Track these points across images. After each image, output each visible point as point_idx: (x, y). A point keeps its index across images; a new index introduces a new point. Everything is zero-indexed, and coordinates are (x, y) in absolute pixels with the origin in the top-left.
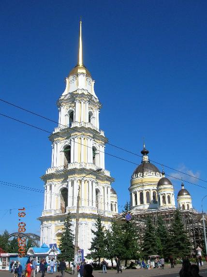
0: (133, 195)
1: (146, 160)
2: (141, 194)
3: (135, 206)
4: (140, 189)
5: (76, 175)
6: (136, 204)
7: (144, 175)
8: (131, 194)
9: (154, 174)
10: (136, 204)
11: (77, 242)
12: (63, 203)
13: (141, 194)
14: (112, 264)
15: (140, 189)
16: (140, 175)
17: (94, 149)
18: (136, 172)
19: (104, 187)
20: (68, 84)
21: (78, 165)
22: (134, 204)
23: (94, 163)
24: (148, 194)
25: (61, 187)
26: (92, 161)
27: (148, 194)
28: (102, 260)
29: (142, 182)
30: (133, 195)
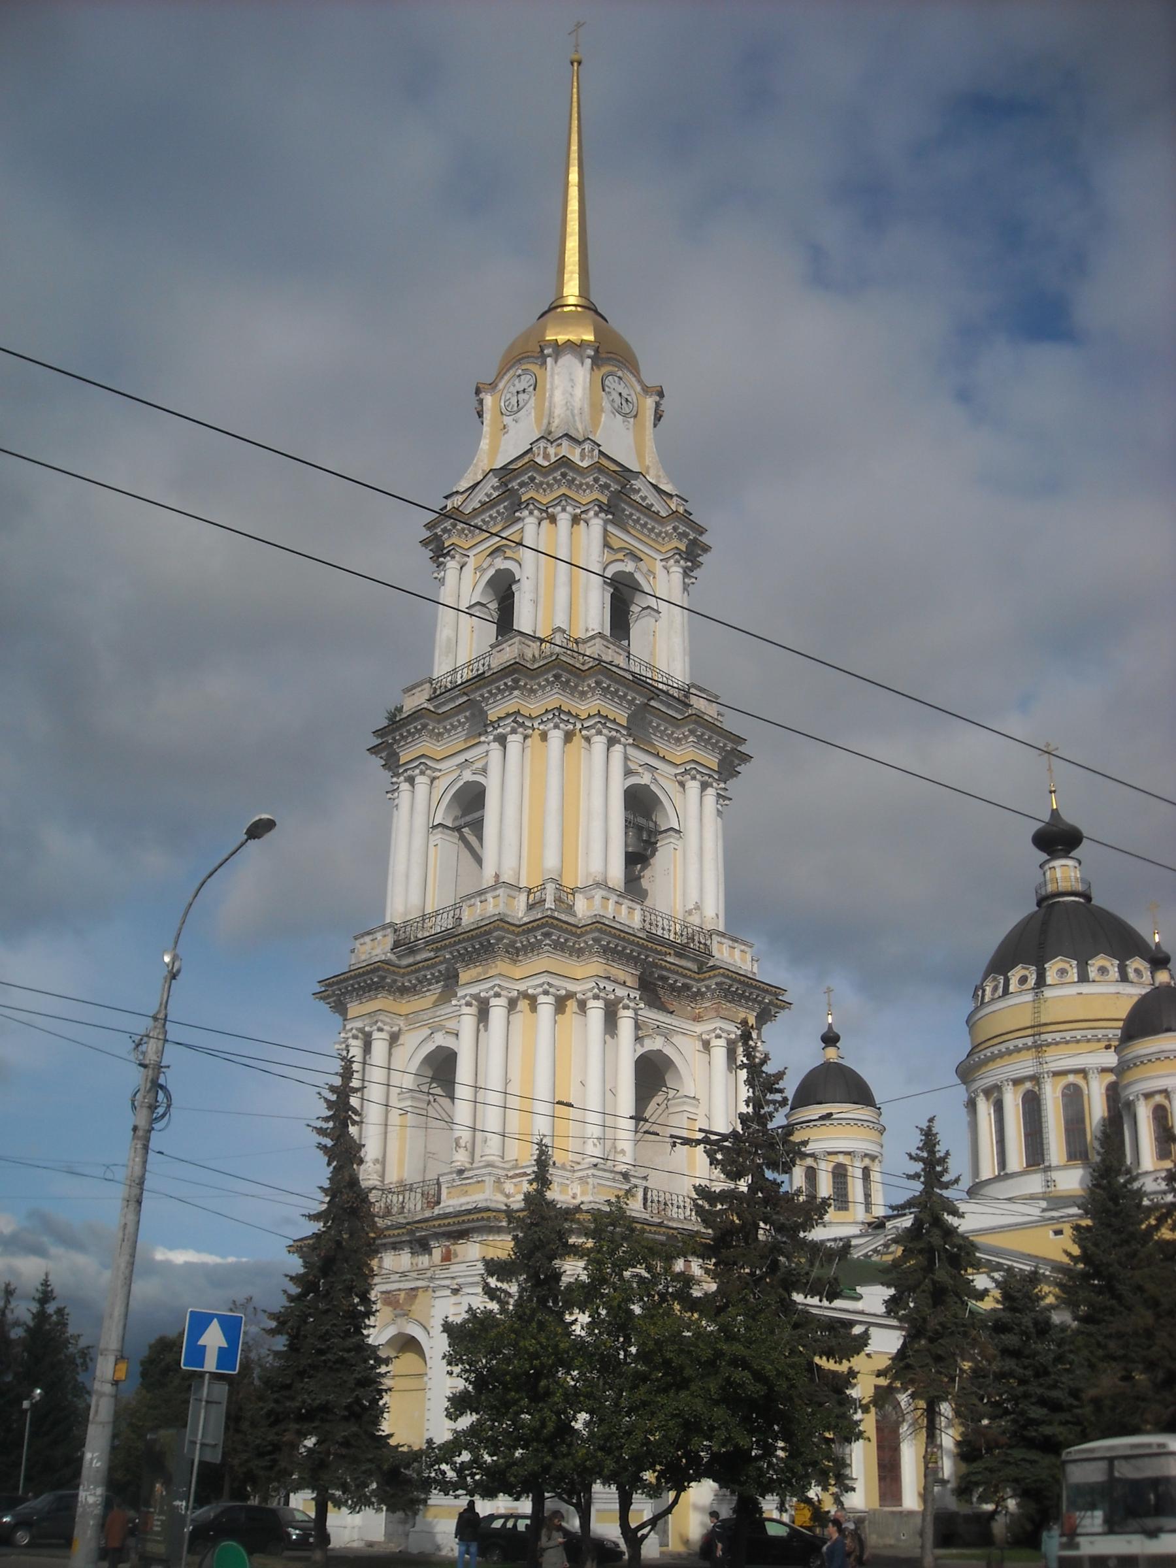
0: (985, 1109)
2: (1033, 1106)
4: (1024, 1065)
6: (1002, 1163)
7: (1051, 977)
8: (972, 1105)
9: (1114, 973)
10: (1002, 1163)
12: (131, 1217)
13: (1033, 1106)
14: (1032, 1197)
15: (1024, 1065)
17: (646, 1132)
18: (1001, 964)
21: (522, 900)
23: (633, 888)
24: (1074, 1099)
26: (616, 873)
27: (1074, 1099)
28: (743, 1186)
29: (1038, 1028)
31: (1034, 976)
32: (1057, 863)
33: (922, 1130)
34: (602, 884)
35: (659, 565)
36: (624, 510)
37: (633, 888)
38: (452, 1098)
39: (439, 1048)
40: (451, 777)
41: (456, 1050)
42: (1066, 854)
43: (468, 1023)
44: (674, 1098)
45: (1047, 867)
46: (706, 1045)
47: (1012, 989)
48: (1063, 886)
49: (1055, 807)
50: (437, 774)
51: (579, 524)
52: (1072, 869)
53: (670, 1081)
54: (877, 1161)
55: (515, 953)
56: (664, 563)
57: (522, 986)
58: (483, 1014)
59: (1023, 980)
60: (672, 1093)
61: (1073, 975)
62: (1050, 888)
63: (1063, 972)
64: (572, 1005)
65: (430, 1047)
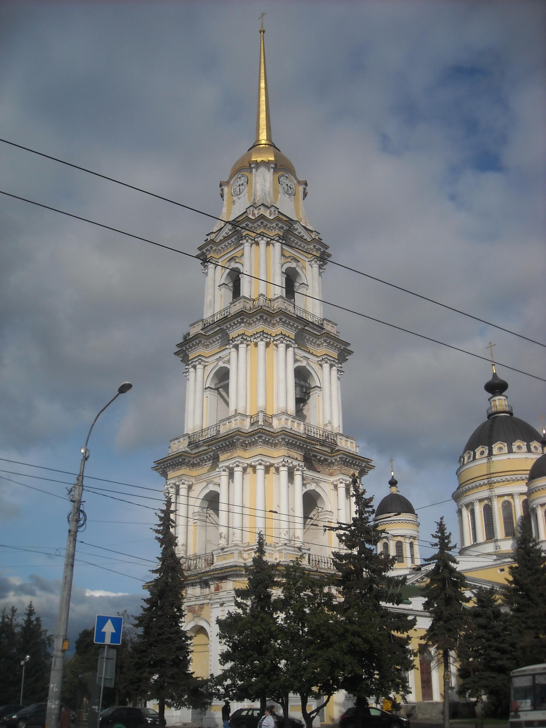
0: (466, 514)
1: (497, 403)
3: (473, 546)
5: (239, 452)
6: (475, 539)
7: (495, 451)
8: (460, 512)
9: (524, 449)
10: (475, 539)
11: (404, 701)
15: (484, 493)
16: (500, 449)
18: (471, 446)
19: (336, 487)
20: (107, 651)
21: (248, 421)
22: (468, 542)
23: (300, 414)
24: (507, 508)
25: (207, 491)
26: (292, 408)
27: (507, 508)
29: (490, 475)
30: (466, 514)
31: (487, 451)
32: (496, 398)
34: (285, 413)
37: (300, 414)
40: (213, 365)
42: (500, 394)
43: (224, 479)
44: (321, 512)
47: (477, 457)
48: (499, 409)
50: (207, 364)
55: (245, 446)
56: (310, 263)
57: (249, 462)
58: (231, 475)
59: (482, 453)
60: (320, 510)
62: (494, 410)
64: (272, 470)
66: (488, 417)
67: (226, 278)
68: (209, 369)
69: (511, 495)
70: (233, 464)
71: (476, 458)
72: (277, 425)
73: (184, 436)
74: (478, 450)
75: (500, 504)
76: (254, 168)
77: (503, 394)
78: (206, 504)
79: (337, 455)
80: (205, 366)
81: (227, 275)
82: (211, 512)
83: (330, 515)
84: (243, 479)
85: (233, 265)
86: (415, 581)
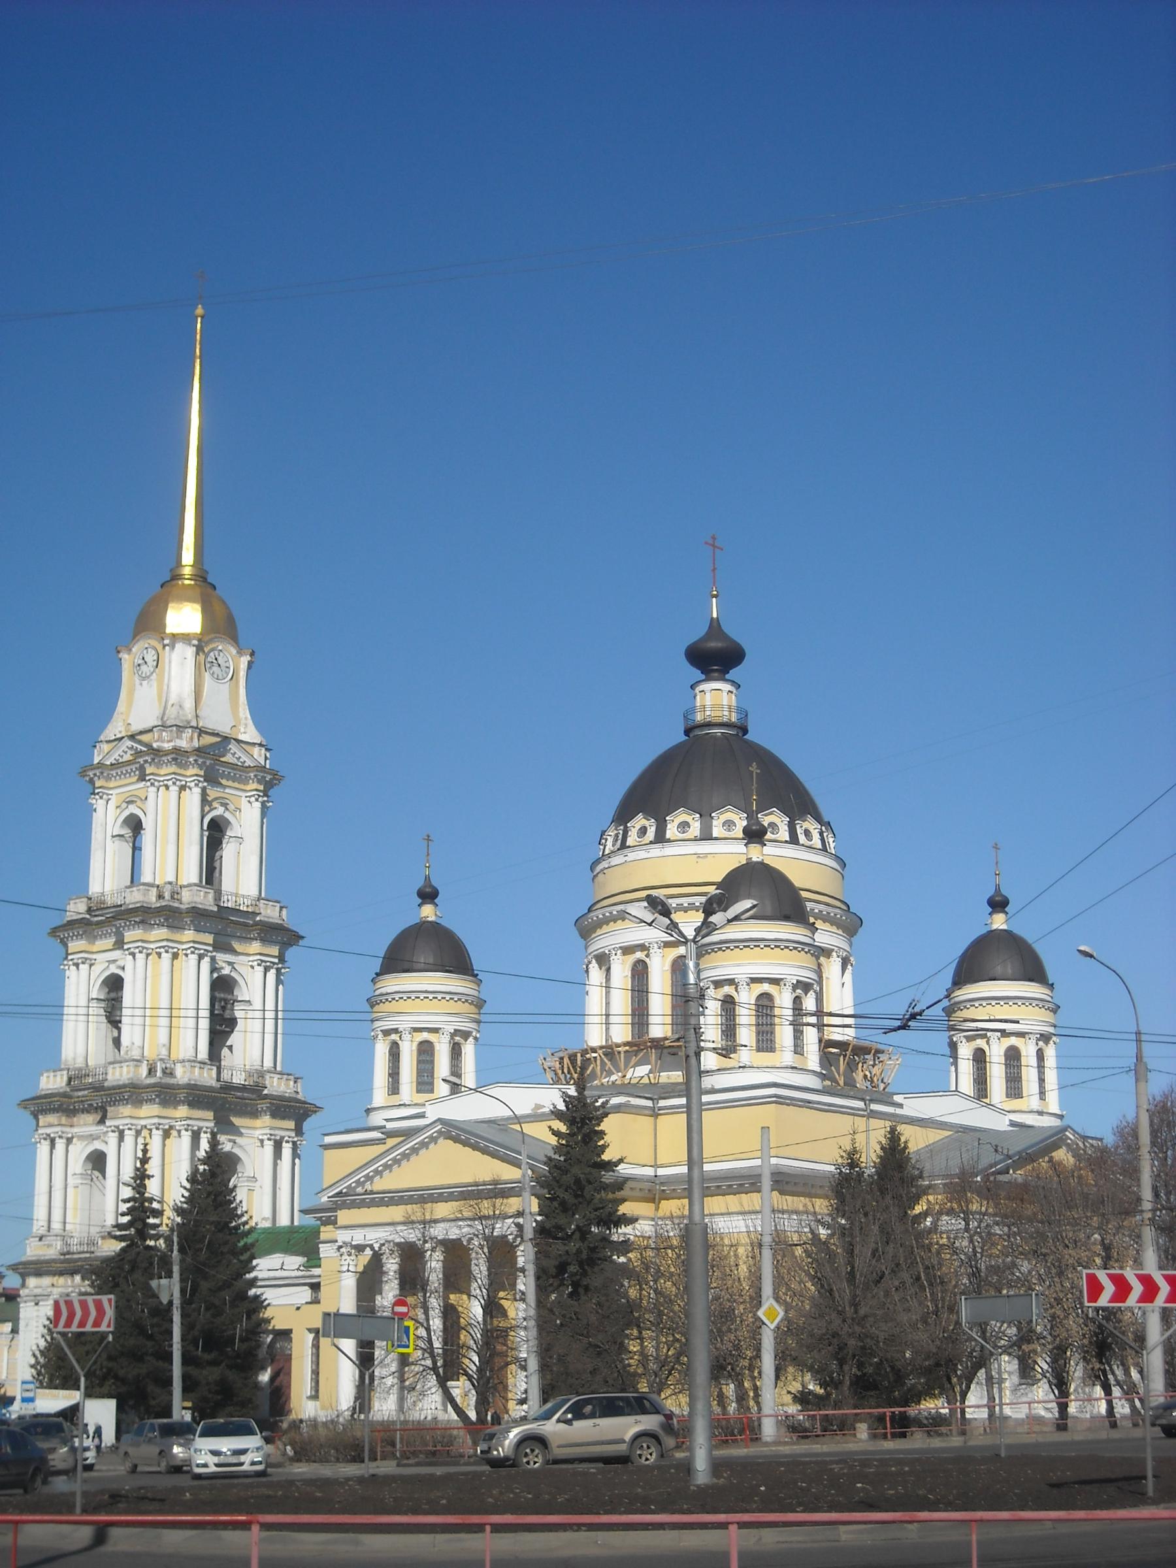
18: (623, 816)
21: (144, 1071)
31: (653, 829)
32: (707, 686)
33: (338, 1310)
34: (194, 1061)
35: (244, 801)
36: (219, 770)
37: (214, 1055)
38: (104, 1177)
39: (96, 1150)
40: (100, 971)
41: (106, 1151)
42: (722, 675)
43: (113, 1138)
44: (242, 1177)
45: (698, 689)
46: (262, 1141)
47: (629, 842)
48: (710, 714)
49: (715, 615)
50: (110, 797)
51: (185, 790)
52: (725, 694)
53: (239, 1168)
54: (471, 1039)
55: (138, 1102)
56: (248, 799)
57: (143, 1122)
58: (121, 1138)
59: (643, 831)
60: (240, 1175)
61: (695, 828)
62: (699, 717)
63: (684, 826)
64: (174, 1133)
65: (107, 973)
66: (687, 732)
67: (122, 826)
68: (97, 969)
69: (775, 982)
70: (124, 1125)
71: (627, 844)
72: (182, 1075)
73: (61, 1070)
74: (639, 821)
75: (627, 968)
76: (168, 645)
77: (727, 676)
78: (90, 1166)
79: (263, 1104)
80: (91, 965)
81: (85, 1161)
82: (96, 1173)
83: (252, 1181)
84: (173, 965)
85: (133, 809)
86: (669, 1190)
